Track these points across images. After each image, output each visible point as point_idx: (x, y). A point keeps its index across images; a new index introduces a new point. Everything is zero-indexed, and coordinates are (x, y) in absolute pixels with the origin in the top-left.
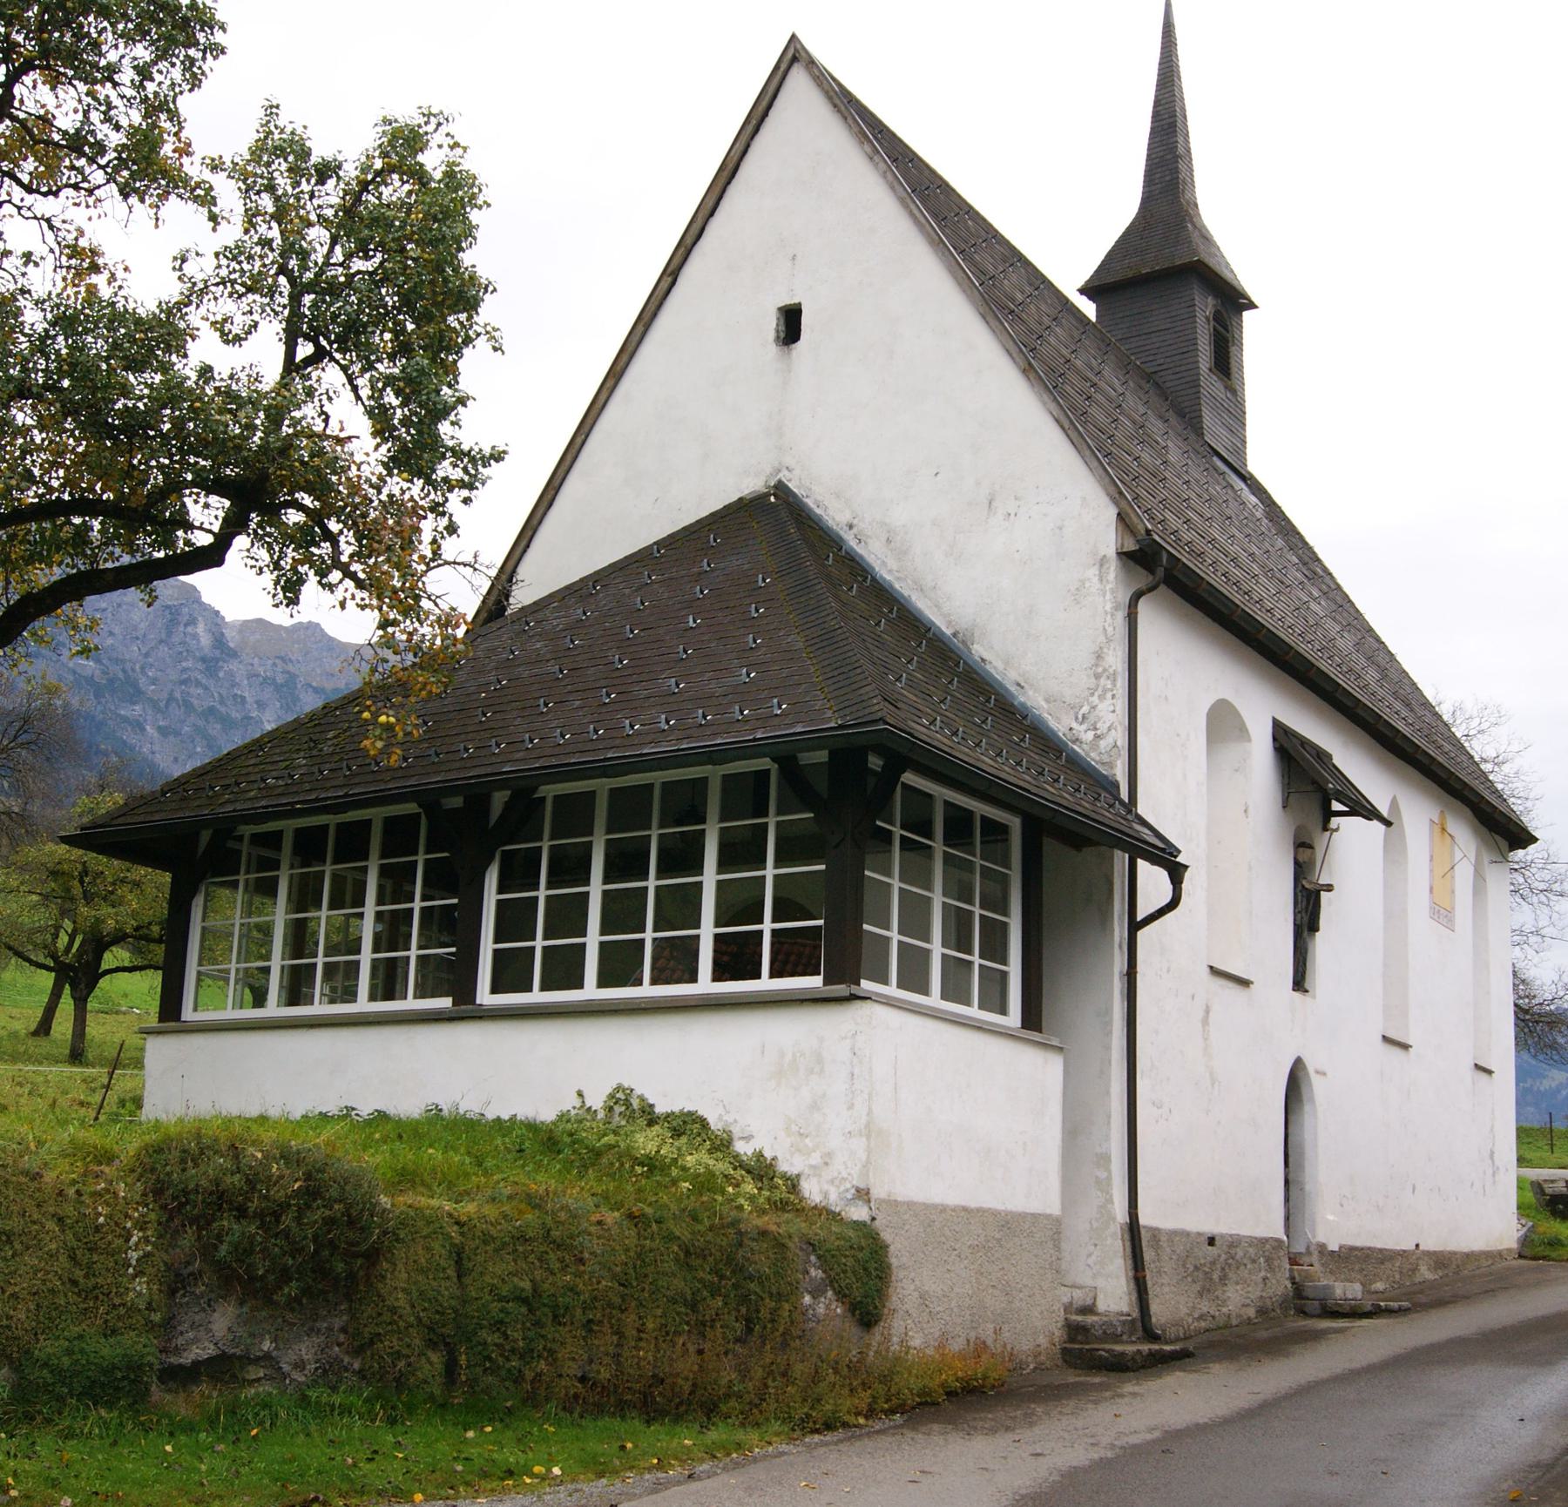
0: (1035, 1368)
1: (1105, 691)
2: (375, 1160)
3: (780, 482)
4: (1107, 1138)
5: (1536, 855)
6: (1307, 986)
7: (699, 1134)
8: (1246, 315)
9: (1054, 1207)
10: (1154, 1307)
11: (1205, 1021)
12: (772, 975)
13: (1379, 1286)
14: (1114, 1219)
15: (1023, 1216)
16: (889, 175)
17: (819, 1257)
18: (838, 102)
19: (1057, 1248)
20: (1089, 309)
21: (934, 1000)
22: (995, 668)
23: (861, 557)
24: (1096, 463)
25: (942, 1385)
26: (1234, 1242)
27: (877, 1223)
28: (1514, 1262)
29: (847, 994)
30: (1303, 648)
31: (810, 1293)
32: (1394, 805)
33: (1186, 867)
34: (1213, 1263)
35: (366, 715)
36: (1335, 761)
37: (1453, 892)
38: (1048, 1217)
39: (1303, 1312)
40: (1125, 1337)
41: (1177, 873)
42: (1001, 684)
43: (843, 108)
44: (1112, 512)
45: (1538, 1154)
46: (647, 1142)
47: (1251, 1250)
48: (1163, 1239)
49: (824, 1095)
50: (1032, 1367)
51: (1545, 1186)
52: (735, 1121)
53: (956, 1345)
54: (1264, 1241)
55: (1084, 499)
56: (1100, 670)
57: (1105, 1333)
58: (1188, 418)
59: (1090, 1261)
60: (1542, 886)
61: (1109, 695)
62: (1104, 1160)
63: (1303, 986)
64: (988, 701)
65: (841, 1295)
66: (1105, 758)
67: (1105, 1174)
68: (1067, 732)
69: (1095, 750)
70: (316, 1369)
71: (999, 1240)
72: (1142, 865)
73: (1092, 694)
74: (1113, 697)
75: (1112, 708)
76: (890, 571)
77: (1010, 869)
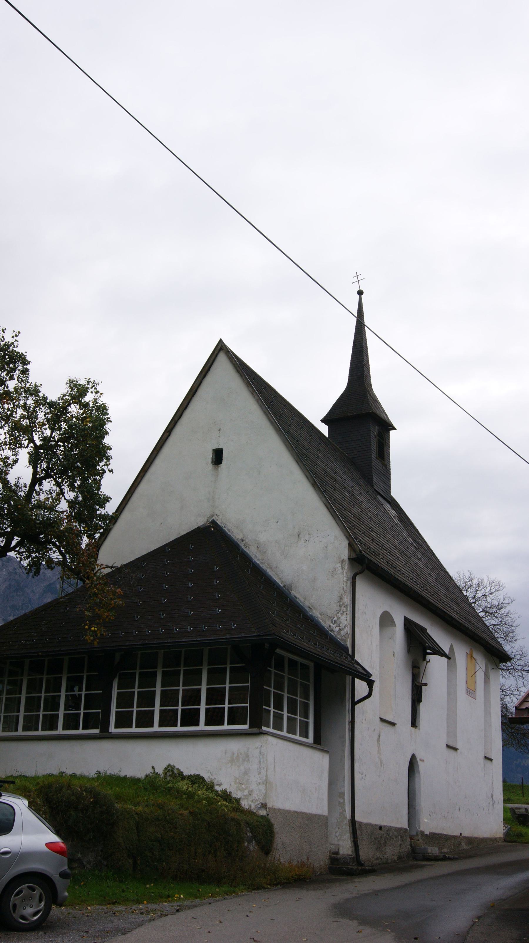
0: (320, 874)
1: (343, 612)
2: (108, 791)
3: (213, 520)
4: (343, 786)
5: (517, 653)
6: (417, 725)
7: (202, 783)
8: (391, 432)
9: (325, 813)
10: (361, 853)
11: (379, 740)
12: (228, 724)
13: (445, 850)
14: (346, 818)
15: (315, 815)
16: (259, 401)
17: (250, 828)
18: (239, 369)
19: (327, 828)
20: (324, 429)
21: (284, 733)
22: (300, 601)
23: (247, 553)
24: (341, 524)
25: (292, 877)
26: (389, 829)
27: (269, 816)
28: (502, 843)
29: (259, 732)
30: (416, 588)
31: (247, 841)
32: (451, 649)
33: (374, 681)
34: (381, 837)
35: (86, 627)
36: (428, 632)
37: (476, 683)
38: (324, 816)
39: (415, 859)
40: (351, 864)
41: (371, 684)
42: (302, 607)
43: (241, 372)
44: (346, 543)
45: (517, 797)
46: (183, 786)
47: (395, 832)
48: (363, 826)
49: (249, 769)
50: (319, 873)
51: (516, 810)
52: (215, 778)
53: (295, 863)
54: (400, 829)
55: (336, 537)
56: (341, 603)
57: (344, 861)
58: (370, 482)
59: (337, 834)
60: (519, 668)
61: (345, 613)
62: (342, 795)
63: (415, 725)
64: (300, 616)
65: (258, 843)
66: (343, 638)
67: (342, 801)
68: (328, 627)
69: (339, 635)
70: (94, 864)
71: (307, 824)
72: (357, 680)
73: (338, 613)
74: (346, 614)
75: (346, 619)
76: (258, 560)
77: (309, 682)
